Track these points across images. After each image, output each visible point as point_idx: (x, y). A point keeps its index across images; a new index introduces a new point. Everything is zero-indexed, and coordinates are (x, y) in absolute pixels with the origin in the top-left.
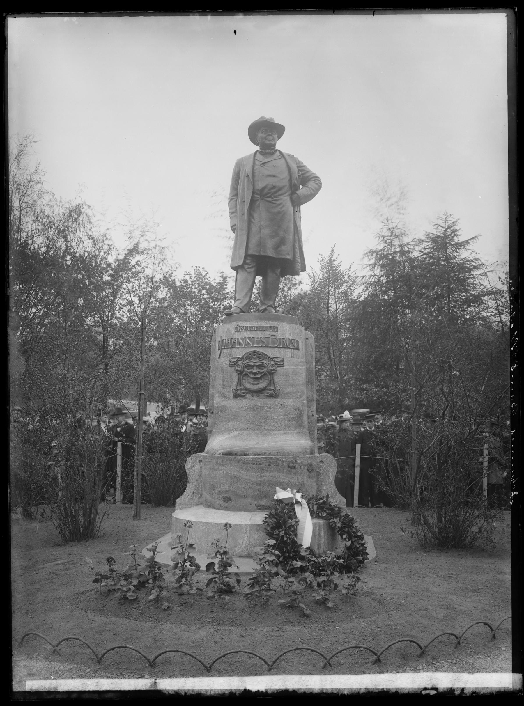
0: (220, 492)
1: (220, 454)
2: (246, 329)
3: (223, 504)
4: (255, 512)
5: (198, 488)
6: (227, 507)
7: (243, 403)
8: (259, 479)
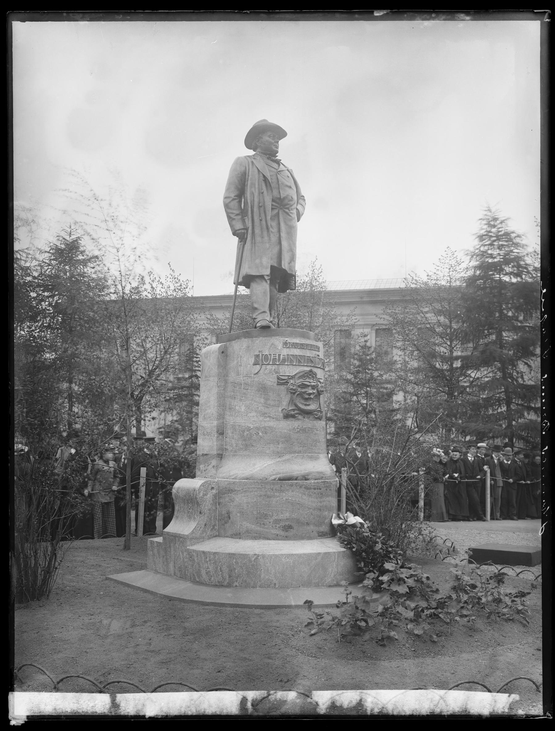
0: (277, 521)
1: (274, 480)
2: (295, 346)
3: (282, 533)
4: (317, 539)
5: (210, 519)
6: (286, 537)
7: (294, 424)
8: (319, 504)
